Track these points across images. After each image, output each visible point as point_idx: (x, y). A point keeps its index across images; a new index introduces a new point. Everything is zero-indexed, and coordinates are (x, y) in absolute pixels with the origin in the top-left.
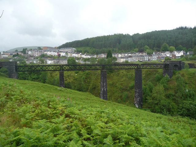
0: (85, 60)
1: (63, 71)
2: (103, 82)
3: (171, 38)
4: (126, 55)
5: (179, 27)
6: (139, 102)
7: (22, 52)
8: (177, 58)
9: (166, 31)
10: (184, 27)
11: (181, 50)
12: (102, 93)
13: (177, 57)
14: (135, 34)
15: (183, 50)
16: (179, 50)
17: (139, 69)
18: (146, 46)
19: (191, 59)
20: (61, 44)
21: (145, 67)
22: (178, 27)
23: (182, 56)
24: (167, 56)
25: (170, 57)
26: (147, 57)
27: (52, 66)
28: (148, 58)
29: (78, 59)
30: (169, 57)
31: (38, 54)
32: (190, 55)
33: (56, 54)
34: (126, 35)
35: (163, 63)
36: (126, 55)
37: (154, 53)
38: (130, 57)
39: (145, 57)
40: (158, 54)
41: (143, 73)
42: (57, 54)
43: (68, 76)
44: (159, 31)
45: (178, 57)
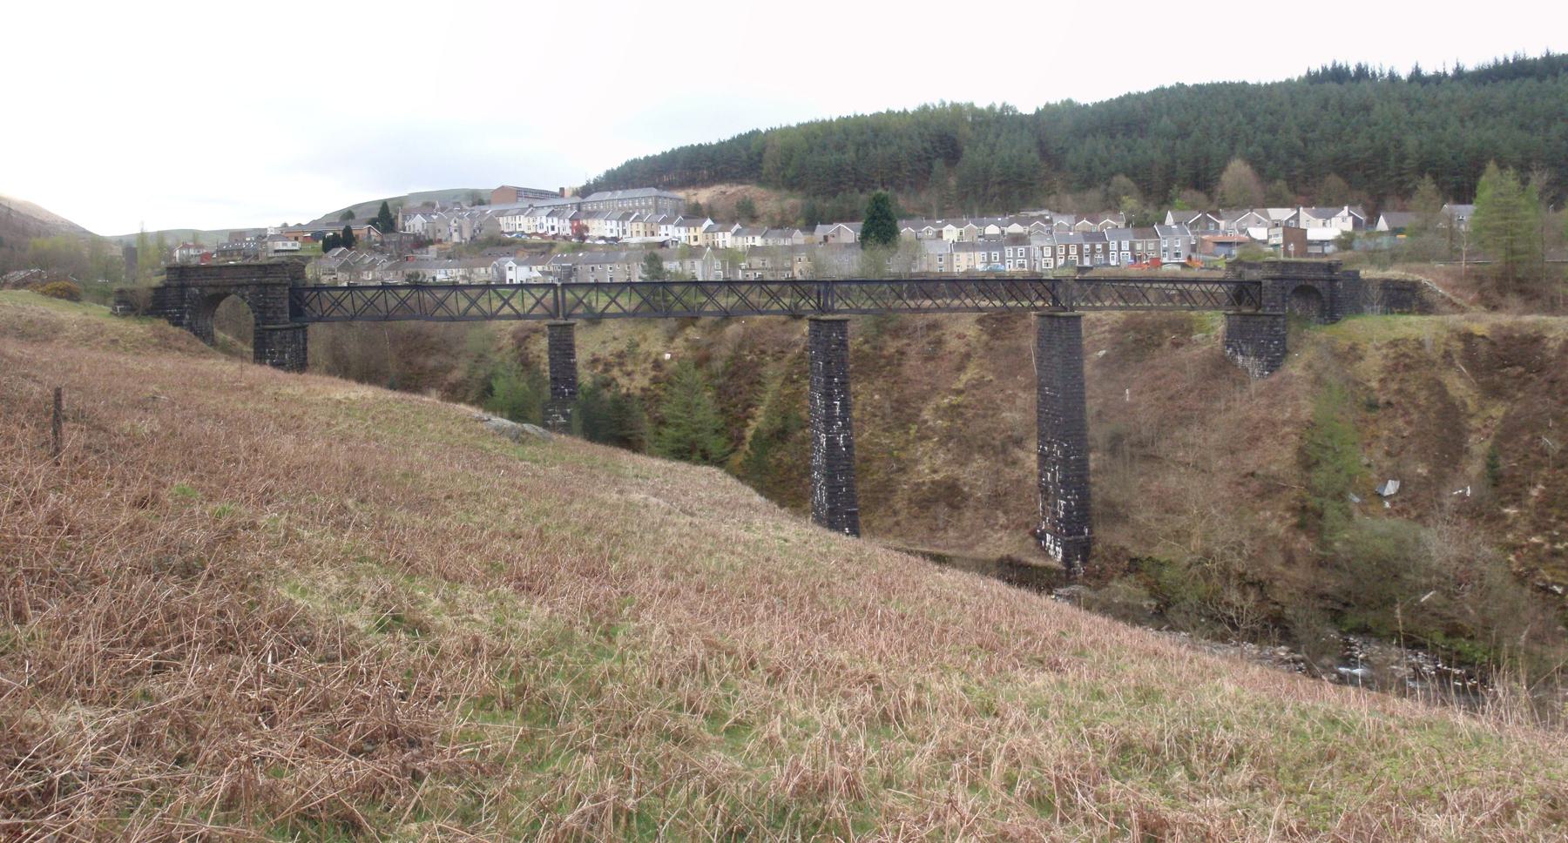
0: (730, 257)
1: (571, 321)
2: (829, 396)
3: (1273, 130)
4: (992, 230)
5: (1325, 69)
6: (1067, 520)
7: (373, 222)
8: (1318, 250)
9: (1232, 85)
10: (1353, 68)
11: (1340, 206)
12: (818, 460)
13: (1312, 243)
14: (1047, 106)
15: (1352, 205)
16: (1326, 204)
17: (1065, 309)
18: (1122, 180)
19: (1394, 257)
20: (596, 171)
21: (530, 301)
22: (1316, 67)
23: (1345, 242)
24: (1254, 240)
25: (1273, 241)
26: (1125, 245)
27: (534, 291)
28: (1132, 248)
29: (692, 252)
30: (1265, 242)
31: (460, 230)
32: (1395, 231)
33: (563, 227)
34: (991, 108)
35: (1219, 275)
36: (992, 230)
37: (1170, 219)
38: (1017, 240)
39: (1113, 246)
40: (1197, 223)
41: (1088, 337)
42: (572, 228)
43: (621, 355)
44: (1199, 89)
45: (1322, 243)
